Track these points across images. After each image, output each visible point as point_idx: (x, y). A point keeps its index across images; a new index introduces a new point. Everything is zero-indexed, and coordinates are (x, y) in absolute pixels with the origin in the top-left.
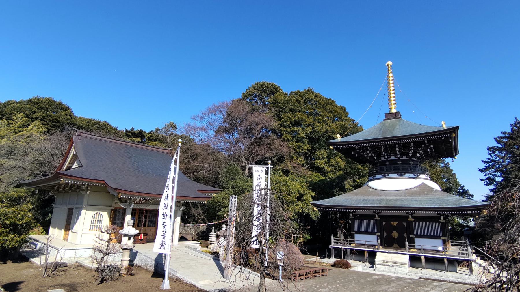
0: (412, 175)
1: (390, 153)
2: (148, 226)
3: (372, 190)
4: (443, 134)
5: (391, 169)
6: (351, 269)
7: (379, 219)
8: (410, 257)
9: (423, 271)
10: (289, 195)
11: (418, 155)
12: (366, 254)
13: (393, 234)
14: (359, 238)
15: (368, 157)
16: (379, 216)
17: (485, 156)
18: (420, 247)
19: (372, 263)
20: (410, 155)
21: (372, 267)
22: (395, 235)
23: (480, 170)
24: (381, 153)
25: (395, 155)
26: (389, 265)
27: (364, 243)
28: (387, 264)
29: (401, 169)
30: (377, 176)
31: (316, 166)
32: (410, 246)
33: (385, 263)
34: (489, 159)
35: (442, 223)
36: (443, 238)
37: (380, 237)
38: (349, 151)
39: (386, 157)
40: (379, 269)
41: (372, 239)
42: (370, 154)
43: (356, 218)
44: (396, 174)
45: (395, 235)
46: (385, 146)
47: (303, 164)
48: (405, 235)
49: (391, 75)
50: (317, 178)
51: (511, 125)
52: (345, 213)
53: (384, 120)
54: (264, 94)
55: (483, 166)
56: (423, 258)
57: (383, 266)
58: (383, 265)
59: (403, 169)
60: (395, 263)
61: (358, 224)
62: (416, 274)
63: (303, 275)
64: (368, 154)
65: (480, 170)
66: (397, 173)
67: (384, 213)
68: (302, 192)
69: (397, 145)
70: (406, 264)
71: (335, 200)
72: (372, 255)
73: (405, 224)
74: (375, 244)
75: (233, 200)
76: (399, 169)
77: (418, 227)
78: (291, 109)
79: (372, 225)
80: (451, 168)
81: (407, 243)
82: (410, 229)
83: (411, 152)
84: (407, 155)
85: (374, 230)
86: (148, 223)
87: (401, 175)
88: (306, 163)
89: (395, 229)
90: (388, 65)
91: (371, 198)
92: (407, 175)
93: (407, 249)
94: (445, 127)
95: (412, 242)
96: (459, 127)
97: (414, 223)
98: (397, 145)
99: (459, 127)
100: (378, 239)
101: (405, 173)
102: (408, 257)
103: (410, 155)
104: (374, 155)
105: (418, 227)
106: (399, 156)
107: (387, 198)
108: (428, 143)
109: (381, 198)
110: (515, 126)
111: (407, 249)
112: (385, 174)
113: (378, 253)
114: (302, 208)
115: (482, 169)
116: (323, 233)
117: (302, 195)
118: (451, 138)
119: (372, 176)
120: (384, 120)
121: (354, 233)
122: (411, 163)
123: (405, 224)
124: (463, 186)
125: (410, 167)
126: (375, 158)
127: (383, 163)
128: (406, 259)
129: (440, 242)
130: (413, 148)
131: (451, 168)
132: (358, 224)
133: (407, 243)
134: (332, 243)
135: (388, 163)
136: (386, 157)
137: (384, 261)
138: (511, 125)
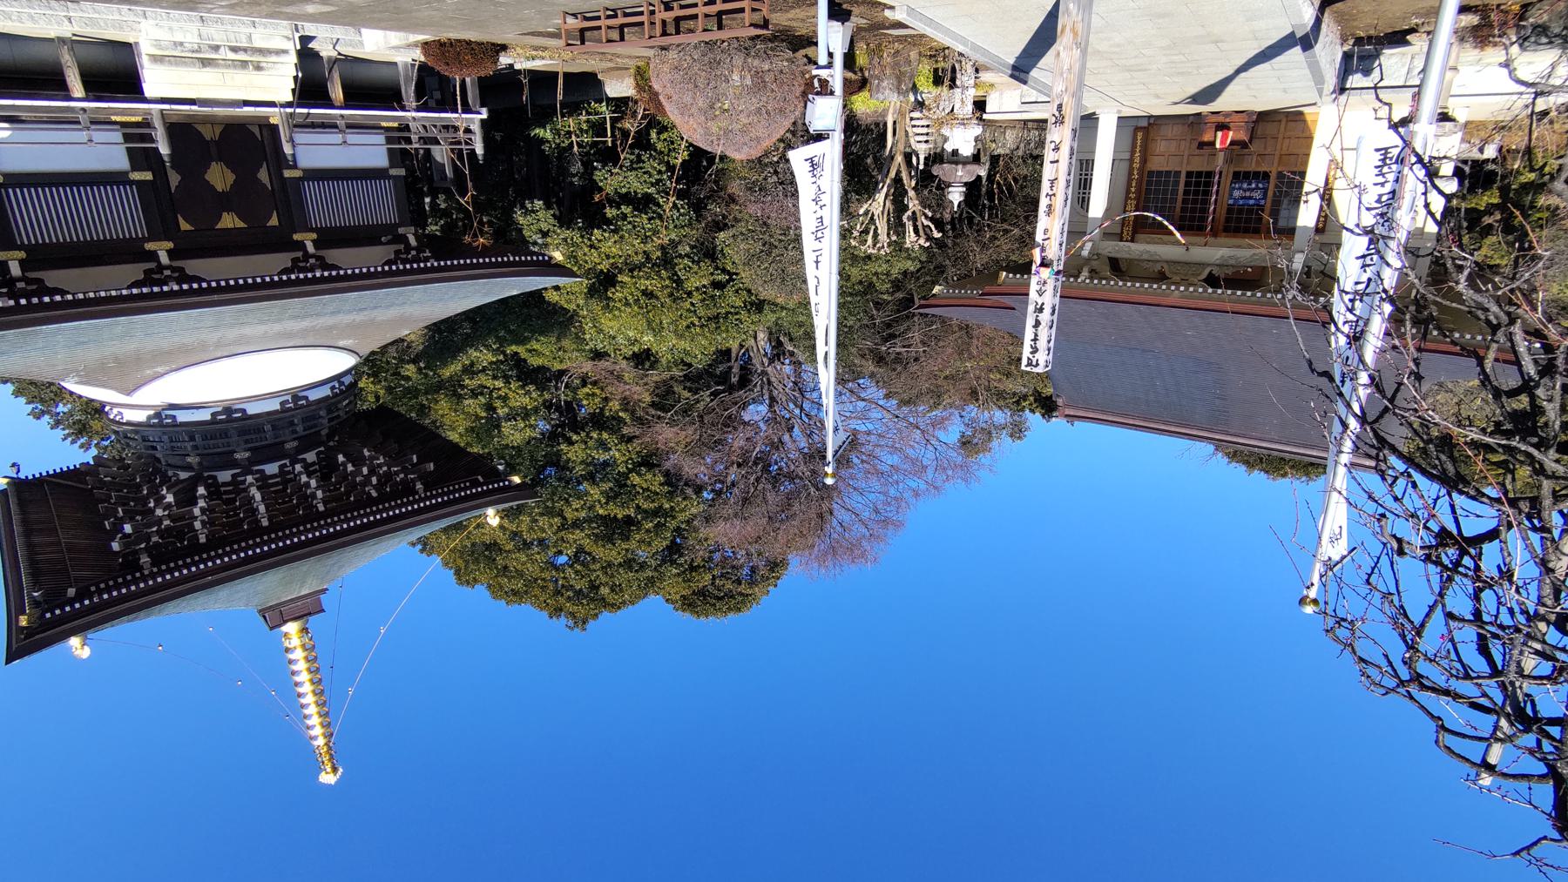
0: (182, 417)
1: (285, 482)
2: (1178, 173)
3: (341, 343)
4: (76, 615)
5: (274, 428)
6: (422, 37)
7: (296, 237)
9: (66, 31)
10: (648, 294)
11: (170, 498)
12: (337, 93)
13: (231, 177)
14: (371, 153)
15: (372, 458)
16: (301, 246)
18: (99, 136)
19: (307, 55)
20: (201, 490)
21: (306, 40)
22: (219, 177)
24: (324, 479)
25: (263, 482)
26: (234, 49)
27: (353, 138)
28: (242, 56)
29: (232, 433)
30: (325, 392)
32: (149, 138)
33: (252, 58)
37: (280, 161)
38: (456, 475)
39: (298, 467)
40: (278, 36)
41: (314, 152)
42: (365, 470)
43: (390, 229)
44: (312, 398)
45: (219, 177)
46: (313, 516)
47: (584, 384)
48: (174, 179)
49: (321, 741)
50: (536, 346)
52: (446, 253)
53: (324, 591)
54: (718, 589)
56: (77, 89)
57: (258, 44)
58: (261, 51)
59: (225, 434)
60: (206, 63)
61: (382, 206)
62: (109, 24)
63: (706, 16)
64: (372, 472)
66: (246, 417)
67: (270, 265)
68: (596, 306)
69: (265, 523)
70: (156, 59)
71: (486, 294)
72: (310, 89)
73: (185, 226)
74: (301, 137)
75: (1042, 357)
76: (243, 432)
77: (121, 216)
79: (323, 208)
80: (23, 400)
81: (164, 150)
82: (160, 205)
83: (202, 503)
84: (215, 490)
85: (311, 190)
86: (1177, 183)
87: (228, 410)
88: (575, 390)
89: (224, 202)
90: (335, 770)
91: (346, 319)
92: (205, 416)
93: (157, 123)
94: (75, 641)
95: (142, 156)
96: (8, 661)
98: (265, 523)
99: (8, 661)
100: (294, 155)
102: (149, 92)
103: (201, 490)
104: (350, 468)
105: (121, 216)
106: (250, 479)
107: (277, 327)
108: (136, 552)
109: (305, 324)
111: (157, 123)
114: (591, 246)
116: (508, 162)
117: (592, 292)
118: (36, 603)
119: (344, 388)
120: (324, 591)
121: (393, 172)
122: (192, 460)
123: (185, 226)
125: (195, 447)
126: (341, 458)
127: (306, 444)
128: (157, 81)
130: (198, 525)
131: (23, 400)
132: (382, 206)
133: (164, 150)
134: (476, 127)
135: (287, 446)
136: (298, 467)
137: (258, 68)
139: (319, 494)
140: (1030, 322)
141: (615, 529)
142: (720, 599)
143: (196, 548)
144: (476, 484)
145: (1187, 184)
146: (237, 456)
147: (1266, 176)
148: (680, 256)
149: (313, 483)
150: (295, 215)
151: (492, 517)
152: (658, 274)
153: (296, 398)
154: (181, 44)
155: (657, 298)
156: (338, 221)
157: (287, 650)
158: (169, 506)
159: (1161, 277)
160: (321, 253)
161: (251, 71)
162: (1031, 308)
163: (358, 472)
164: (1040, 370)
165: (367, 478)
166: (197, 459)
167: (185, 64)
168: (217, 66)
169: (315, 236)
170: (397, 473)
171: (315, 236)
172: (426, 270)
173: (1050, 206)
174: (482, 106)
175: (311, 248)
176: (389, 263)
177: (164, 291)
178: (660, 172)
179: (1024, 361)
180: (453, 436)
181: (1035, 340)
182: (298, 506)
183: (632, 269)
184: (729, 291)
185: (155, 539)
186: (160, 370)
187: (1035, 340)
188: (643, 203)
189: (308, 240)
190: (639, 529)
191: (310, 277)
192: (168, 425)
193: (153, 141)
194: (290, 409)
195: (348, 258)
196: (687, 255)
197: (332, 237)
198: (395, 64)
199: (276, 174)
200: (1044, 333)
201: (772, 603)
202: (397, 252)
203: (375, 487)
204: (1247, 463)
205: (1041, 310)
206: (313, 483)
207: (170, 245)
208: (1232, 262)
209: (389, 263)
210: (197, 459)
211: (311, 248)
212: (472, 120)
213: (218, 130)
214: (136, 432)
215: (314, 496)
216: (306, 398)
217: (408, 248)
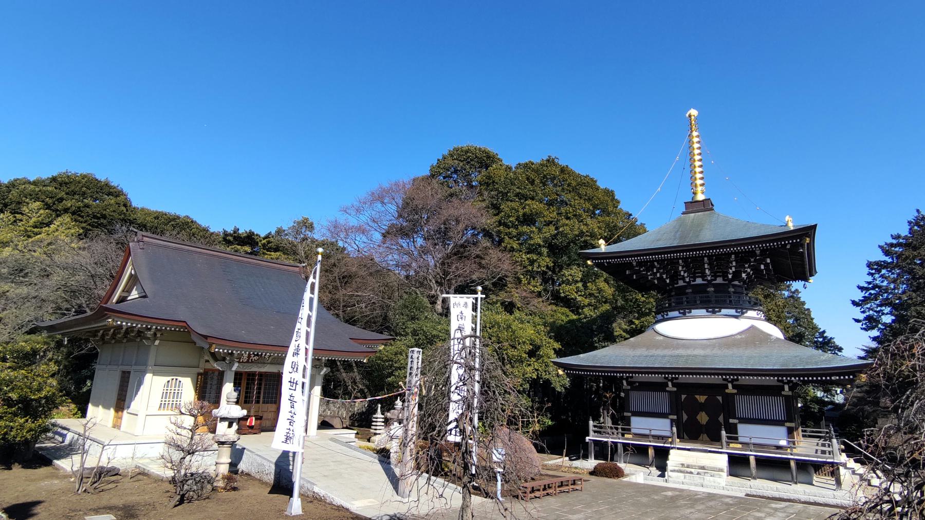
0: (732, 312)
1: (695, 273)
2: (264, 403)
3: (662, 338)
4: (788, 239)
5: (695, 302)
6: (625, 479)
7: (675, 389)
8: (729, 457)
9: (753, 482)
10: (514, 347)
11: (744, 275)
12: (651, 452)
13: (698, 417)
14: (639, 424)
15: (654, 279)
16: (674, 385)
17: (864, 278)
18: (746, 440)
19: (662, 469)
20: (730, 276)
21: (662, 475)
22: (703, 418)
23: (854, 303)
24: (677, 272)
25: (703, 276)
26: (691, 473)
27: (647, 432)
28: (689, 470)
29: (714, 300)
30: (671, 314)
31: (562, 295)
32: (729, 438)
33: (685, 469)
34: (869, 283)
35: (787, 397)
36: (788, 424)
37: (676, 423)
39: (687, 280)
40: (675, 480)
41: (662, 426)
42: (658, 275)
43: (634, 388)
44: (704, 311)
45: (703, 418)
46: (685, 259)
47: (540, 293)
48: (721, 419)
49: (695, 134)
50: (564, 318)
51: (910, 223)
52: (613, 379)
53: (683, 213)
54: (469, 167)
55: (859, 296)
56: (752, 459)
57: (682, 475)
58: (681, 472)
59: (717, 302)
60: (703, 468)
61: (637, 399)
63: (539, 490)
64: (655, 274)
65: (854, 303)
66: (707, 308)
67: (683, 379)
68: (538, 342)
69: (706, 259)
70: (722, 470)
71: (596, 356)
72: (662, 455)
73: (720, 398)
74: (668, 434)
75: (415, 355)
76: (710, 302)
77: (744, 405)
78: (517, 195)
79: (662, 401)
80: (802, 300)
81: (724, 433)
82: (729, 408)
83: (731, 271)
84: (725, 276)
85: (666, 409)
86: (264, 398)
87: (714, 312)
88: (545, 290)
89: (702, 407)
90: (690, 116)
91: (659, 352)
92: (724, 311)
93: (724, 444)
94: (791, 226)
95: (732, 431)
96: (816, 225)
97: (737, 398)
98: (706, 259)
99: (816, 225)
100: (672, 426)
101: (721, 308)
102: (726, 457)
103: (730, 276)
104: (664, 276)
105: (744, 405)
106: (709, 278)
107: (689, 352)
108: (761, 255)
109: (677, 352)
110: (917, 224)
111: (724, 444)
112: (684, 309)
113: (672, 451)
114: (537, 370)
115: (857, 300)
116: (574, 415)
117: (537, 348)
118: (802, 246)
119: (662, 313)
120: (683, 213)
121: (629, 414)
122: (732, 290)
123: (720, 398)
124: (824, 332)
125: (730, 297)
126: (668, 281)
127: (681, 291)
128: (722, 461)
129: (782, 430)
130: (734, 264)
131: (802, 300)
132: (637, 399)
133: (724, 433)
134: (591, 433)
135: (690, 290)
136: (687, 280)
137: (683, 465)
138: (910, 223)
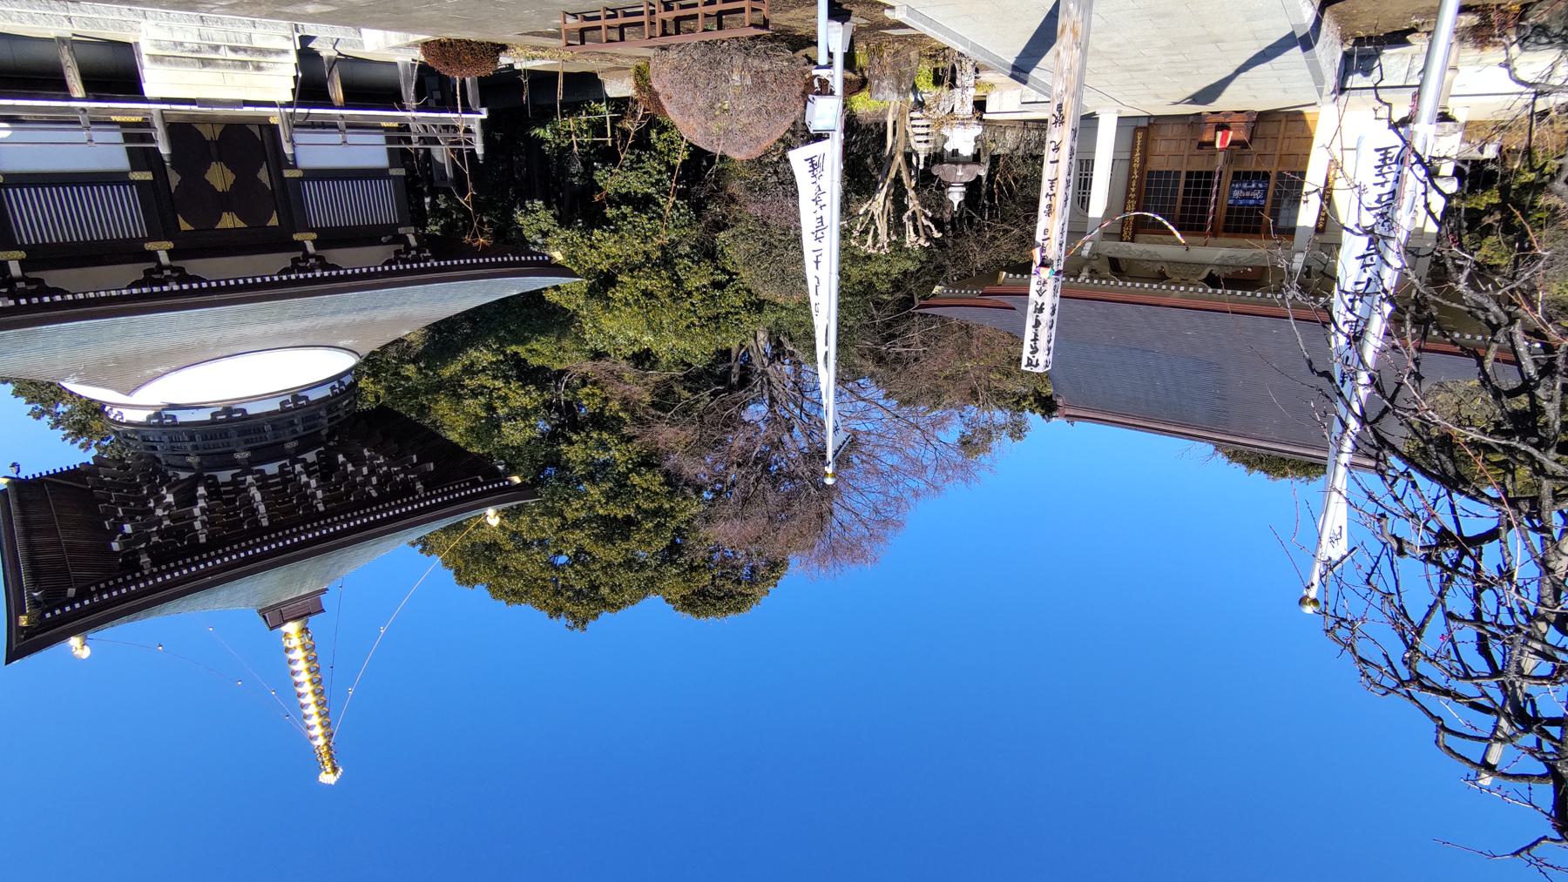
0: (182, 417)
1: (285, 482)
2: (1178, 173)
3: (341, 343)
4: (76, 615)
5: (274, 428)
6: (422, 37)
7: (296, 237)
9: (66, 31)
10: (648, 294)
11: (170, 498)
12: (337, 93)
13: (231, 177)
14: (371, 153)
15: (372, 458)
16: (301, 246)
18: (99, 136)
19: (307, 55)
20: (201, 490)
21: (306, 40)
22: (219, 177)
24: (324, 479)
25: (263, 482)
26: (234, 49)
27: (353, 138)
28: (242, 56)
29: (232, 433)
30: (325, 392)
32: (149, 138)
33: (252, 58)
37: (280, 161)
38: (456, 475)
39: (298, 467)
40: (278, 36)
41: (314, 152)
42: (365, 470)
43: (390, 229)
44: (312, 398)
45: (219, 177)
46: (313, 516)
47: (584, 384)
48: (174, 179)
49: (321, 741)
50: (536, 346)
52: (446, 253)
53: (324, 591)
54: (718, 589)
56: (77, 89)
57: (258, 44)
58: (261, 51)
59: (225, 434)
60: (206, 63)
61: (382, 206)
63: (706, 16)
64: (372, 472)
66: (246, 417)
67: (270, 265)
68: (596, 306)
69: (265, 523)
70: (156, 59)
71: (486, 294)
72: (310, 89)
73: (185, 226)
74: (301, 137)
75: (1042, 357)
76: (243, 432)
77: (121, 216)
79: (323, 208)
80: (23, 400)
81: (164, 150)
82: (160, 205)
83: (202, 503)
84: (215, 490)
85: (311, 190)
86: (1177, 183)
87: (228, 410)
88: (575, 390)
89: (224, 202)
90: (335, 770)
91: (346, 319)
92: (205, 416)
93: (157, 123)
94: (75, 641)
95: (142, 156)
96: (8, 661)
98: (265, 523)
99: (8, 661)
100: (294, 155)
102: (149, 92)
103: (201, 490)
104: (350, 468)
105: (121, 216)
106: (250, 479)
107: (277, 327)
108: (136, 552)
109: (305, 324)
111: (157, 123)
114: (591, 246)
116: (508, 162)
117: (592, 292)
118: (36, 603)
119: (344, 388)
120: (324, 591)
121: (393, 172)
122: (192, 460)
123: (185, 226)
125: (195, 447)
126: (341, 458)
127: (306, 444)
128: (157, 81)
130: (198, 525)
131: (23, 400)
132: (382, 206)
133: (164, 150)
134: (476, 127)
135: (287, 446)
136: (298, 467)
137: (258, 68)
139: (319, 494)
140: (1030, 322)
141: (615, 529)
142: (720, 599)
143: (196, 548)
144: (476, 484)
145: (1187, 184)
146: (237, 456)
147: (1266, 176)
148: (680, 256)
149: (313, 483)
150: (295, 215)
151: (492, 517)
152: (658, 274)
153: (296, 398)
154: (181, 44)
155: (657, 298)
156: (338, 221)
157: (287, 650)
158: (169, 506)
159: (1161, 277)
160: (321, 253)
161: (251, 71)
162: (1031, 308)
163: (358, 472)
164: (1040, 370)
165: (367, 478)
166: (197, 459)
167: (185, 64)
168: (217, 66)
169: (315, 236)
170: (397, 473)
171: (315, 236)
172: (426, 270)
173: (1050, 206)
174: (482, 106)
175: (311, 248)
176: (389, 263)
177: (164, 291)
178: (660, 172)
179: (1024, 361)
180: (453, 436)
181: (1035, 340)
182: (298, 506)
183: (632, 269)
184: (729, 291)
185: (155, 539)
186: (160, 370)
187: (1035, 340)
188: (643, 203)
189: (308, 240)
190: (639, 529)
191: (310, 277)
192: (168, 425)
193: (153, 141)
194: (290, 409)
195: (348, 258)
196: (687, 255)
197: (332, 237)
198: (395, 64)
199: (276, 174)
200: (1044, 333)
201: (772, 603)
202: (397, 252)
203: (375, 487)
204: (1247, 463)
205: (1041, 310)
206: (313, 483)
207: (170, 245)
208: (1232, 262)
209: (389, 263)
210: (197, 459)
211: (311, 248)
212: (472, 120)
213: (218, 130)
214: (136, 432)
215: (314, 496)
216: (306, 398)
217: (408, 248)
